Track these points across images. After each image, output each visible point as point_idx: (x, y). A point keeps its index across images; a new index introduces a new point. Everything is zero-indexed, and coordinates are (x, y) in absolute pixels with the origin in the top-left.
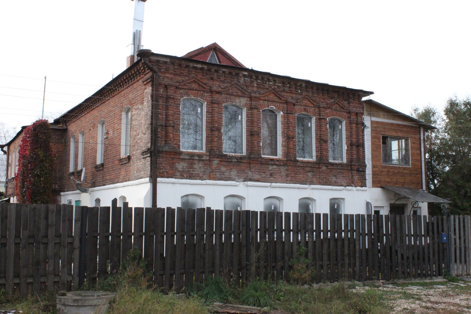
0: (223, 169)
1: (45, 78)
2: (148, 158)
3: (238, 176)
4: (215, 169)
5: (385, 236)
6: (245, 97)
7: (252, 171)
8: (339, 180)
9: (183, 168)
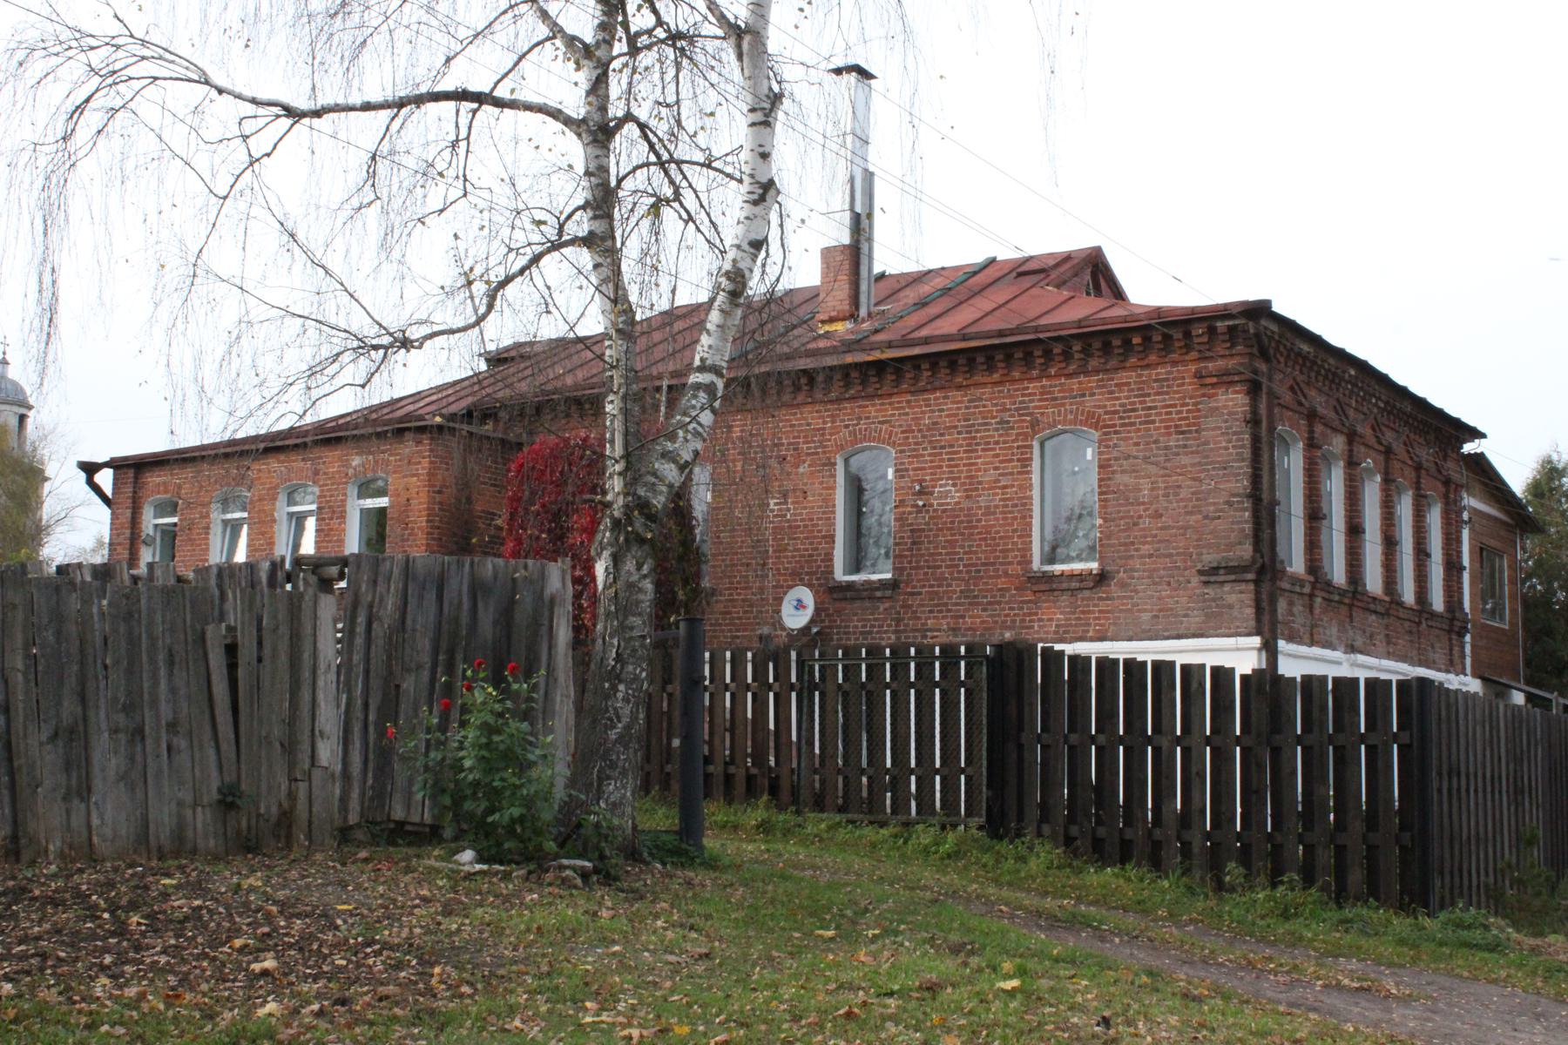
2: (1243, 586)
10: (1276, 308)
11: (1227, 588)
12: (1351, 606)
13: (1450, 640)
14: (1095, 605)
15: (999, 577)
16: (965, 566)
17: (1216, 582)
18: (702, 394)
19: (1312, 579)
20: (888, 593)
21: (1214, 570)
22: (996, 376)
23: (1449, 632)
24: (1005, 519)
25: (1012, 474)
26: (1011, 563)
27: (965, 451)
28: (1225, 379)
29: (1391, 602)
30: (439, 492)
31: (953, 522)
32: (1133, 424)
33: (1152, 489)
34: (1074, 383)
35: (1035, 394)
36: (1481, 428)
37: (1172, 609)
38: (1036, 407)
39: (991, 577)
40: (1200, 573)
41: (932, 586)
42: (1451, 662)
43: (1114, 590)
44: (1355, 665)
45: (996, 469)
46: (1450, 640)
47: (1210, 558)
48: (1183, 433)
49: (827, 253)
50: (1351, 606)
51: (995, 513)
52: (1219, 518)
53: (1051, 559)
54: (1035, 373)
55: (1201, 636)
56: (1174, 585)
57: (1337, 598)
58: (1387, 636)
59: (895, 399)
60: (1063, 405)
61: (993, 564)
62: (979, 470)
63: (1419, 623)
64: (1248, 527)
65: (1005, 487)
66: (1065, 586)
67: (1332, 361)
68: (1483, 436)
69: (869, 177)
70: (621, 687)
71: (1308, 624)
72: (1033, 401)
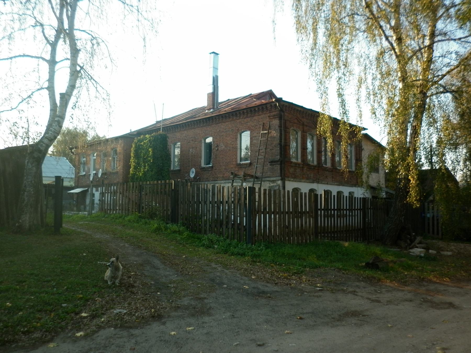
0: (308, 173)
10: (283, 99)
11: (275, 166)
12: (318, 170)
15: (231, 165)
18: (56, 123)
20: (211, 169)
22: (231, 119)
28: (274, 117)
30: (125, 151)
34: (245, 120)
36: (366, 128)
40: (269, 162)
49: (208, 94)
50: (318, 170)
53: (241, 161)
54: (238, 118)
57: (313, 168)
58: (332, 176)
59: (213, 126)
64: (279, 151)
65: (232, 144)
66: (243, 166)
68: (367, 129)
69: (217, 77)
70: (26, 193)
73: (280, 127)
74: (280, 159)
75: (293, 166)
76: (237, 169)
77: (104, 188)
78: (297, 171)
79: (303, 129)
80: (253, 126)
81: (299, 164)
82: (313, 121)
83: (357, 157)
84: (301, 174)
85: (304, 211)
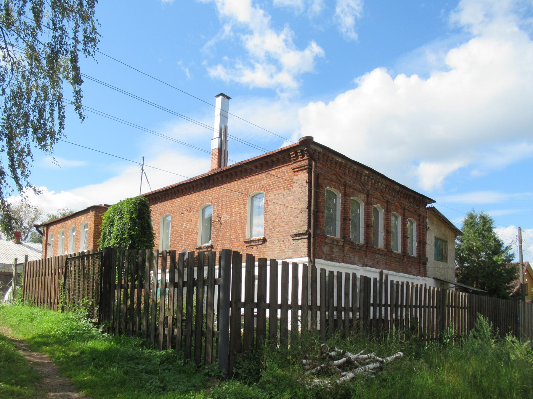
0: (351, 255)
1: (143, 158)
2: (304, 240)
3: (359, 261)
4: (347, 254)
5: (301, 309)
6: (363, 193)
7: (367, 258)
8: (412, 271)
9: (327, 251)
10: (315, 140)
13: (419, 266)
14: (262, 250)
15: (237, 242)
16: (229, 239)
17: (296, 240)
19: (343, 240)
21: (296, 235)
23: (419, 263)
24: (240, 223)
25: (242, 209)
26: (241, 238)
27: (230, 203)
28: (300, 169)
29: (387, 251)
31: (226, 226)
32: (274, 188)
33: (279, 210)
35: (248, 182)
36: (434, 200)
37: (284, 250)
38: (249, 186)
39: (235, 242)
40: (292, 236)
41: (221, 246)
42: (420, 273)
43: (267, 244)
44: (366, 270)
45: (238, 208)
46: (419, 266)
47: (295, 231)
48: (288, 189)
50: (366, 251)
51: (237, 222)
52: (298, 217)
55: (292, 258)
56: (285, 241)
57: (357, 248)
58: (386, 262)
60: (256, 184)
61: (236, 238)
62: (233, 208)
63: (403, 259)
66: (254, 244)
67: (355, 167)
68: (435, 202)
71: (342, 255)
72: (247, 184)
73: (309, 183)
74: (307, 231)
75: (328, 243)
76: (245, 248)
77: (371, 317)
78: (334, 250)
79: (345, 191)
80: (270, 185)
81: (338, 241)
82: (360, 181)
83: (419, 239)
84: (340, 256)
85: (343, 306)
